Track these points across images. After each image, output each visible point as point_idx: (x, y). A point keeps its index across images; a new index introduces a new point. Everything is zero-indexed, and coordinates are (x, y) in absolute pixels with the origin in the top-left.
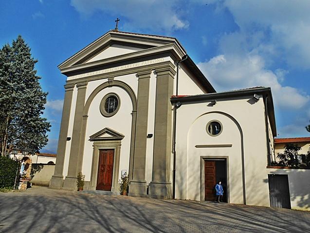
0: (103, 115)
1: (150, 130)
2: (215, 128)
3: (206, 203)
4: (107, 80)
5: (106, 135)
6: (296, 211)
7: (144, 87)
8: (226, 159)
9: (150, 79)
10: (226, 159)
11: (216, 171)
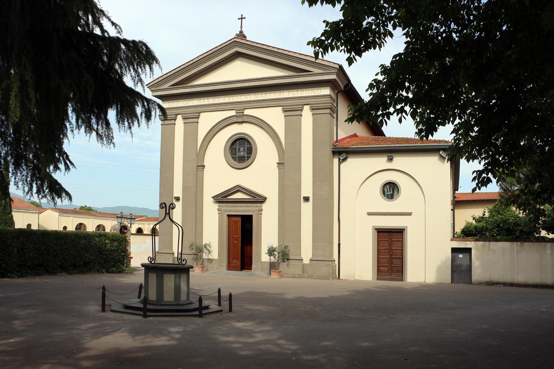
0: (233, 167)
1: (307, 189)
2: (391, 190)
4: (233, 113)
5: (239, 196)
7: (294, 130)
9: (302, 118)
10: (404, 229)
11: (390, 245)
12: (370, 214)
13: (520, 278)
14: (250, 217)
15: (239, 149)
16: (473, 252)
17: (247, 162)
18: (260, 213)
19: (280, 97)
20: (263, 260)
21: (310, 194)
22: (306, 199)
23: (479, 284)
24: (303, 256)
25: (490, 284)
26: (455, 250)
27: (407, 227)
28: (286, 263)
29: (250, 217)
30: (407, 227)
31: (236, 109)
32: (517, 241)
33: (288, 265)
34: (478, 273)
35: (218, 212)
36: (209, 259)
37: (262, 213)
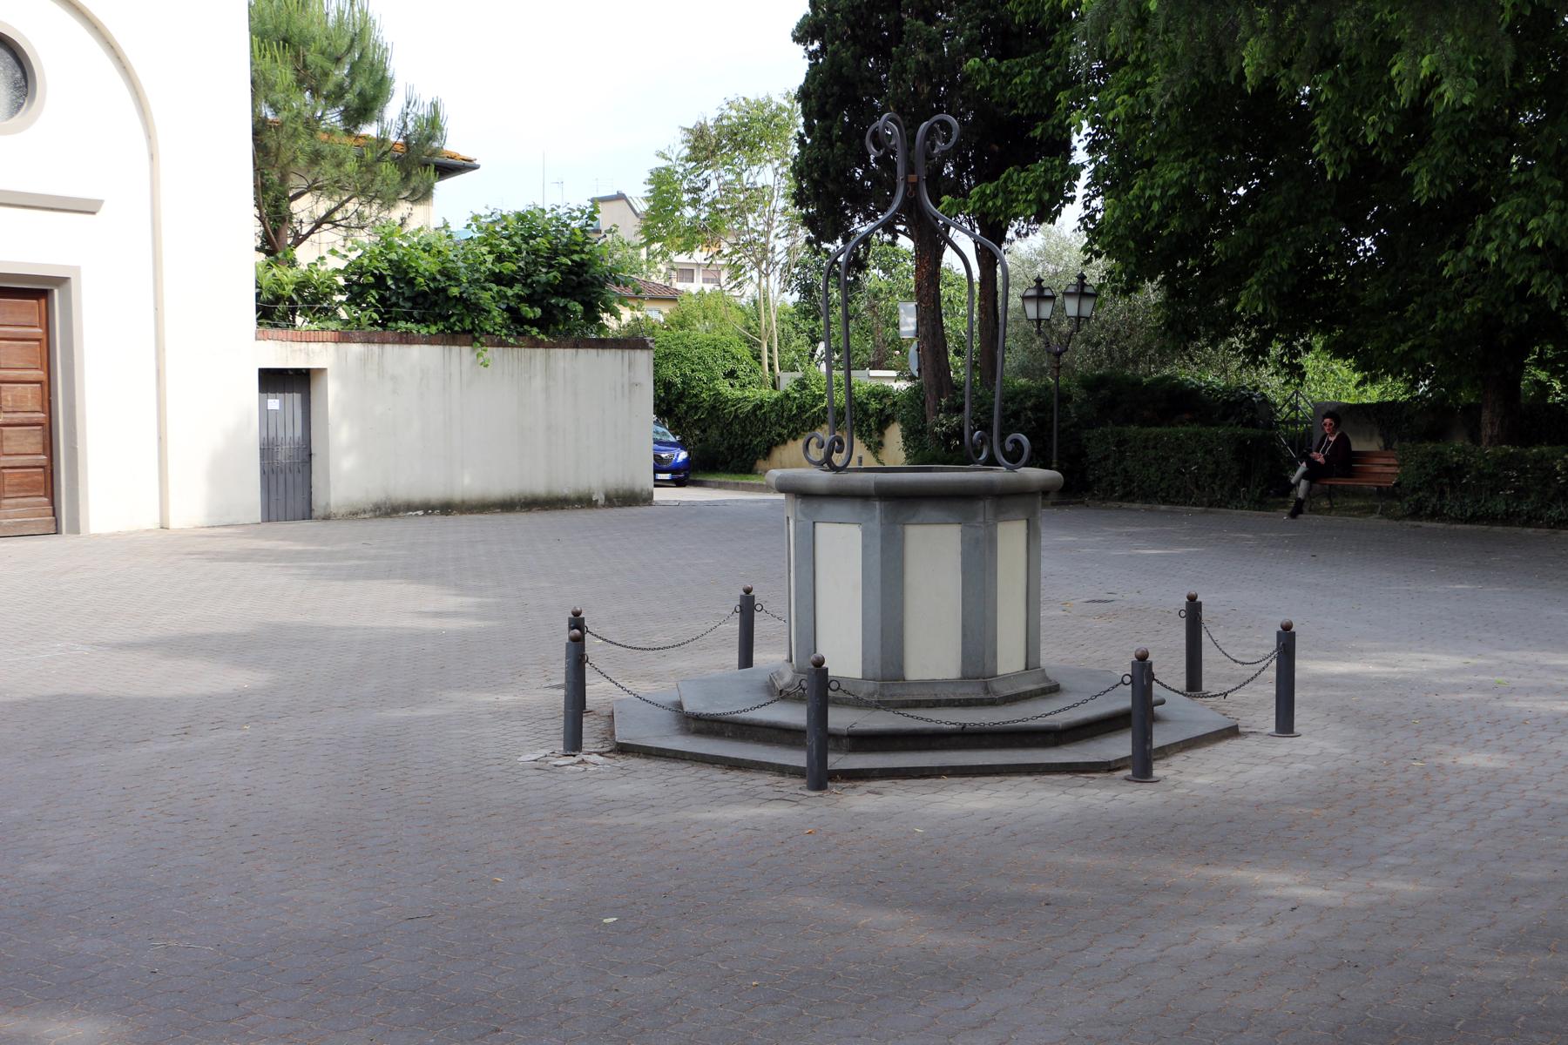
6: (386, 525)
10: (62, 281)
13: (468, 484)
23: (354, 514)
26: (272, 380)
27: (77, 269)
30: (77, 269)
34: (347, 468)
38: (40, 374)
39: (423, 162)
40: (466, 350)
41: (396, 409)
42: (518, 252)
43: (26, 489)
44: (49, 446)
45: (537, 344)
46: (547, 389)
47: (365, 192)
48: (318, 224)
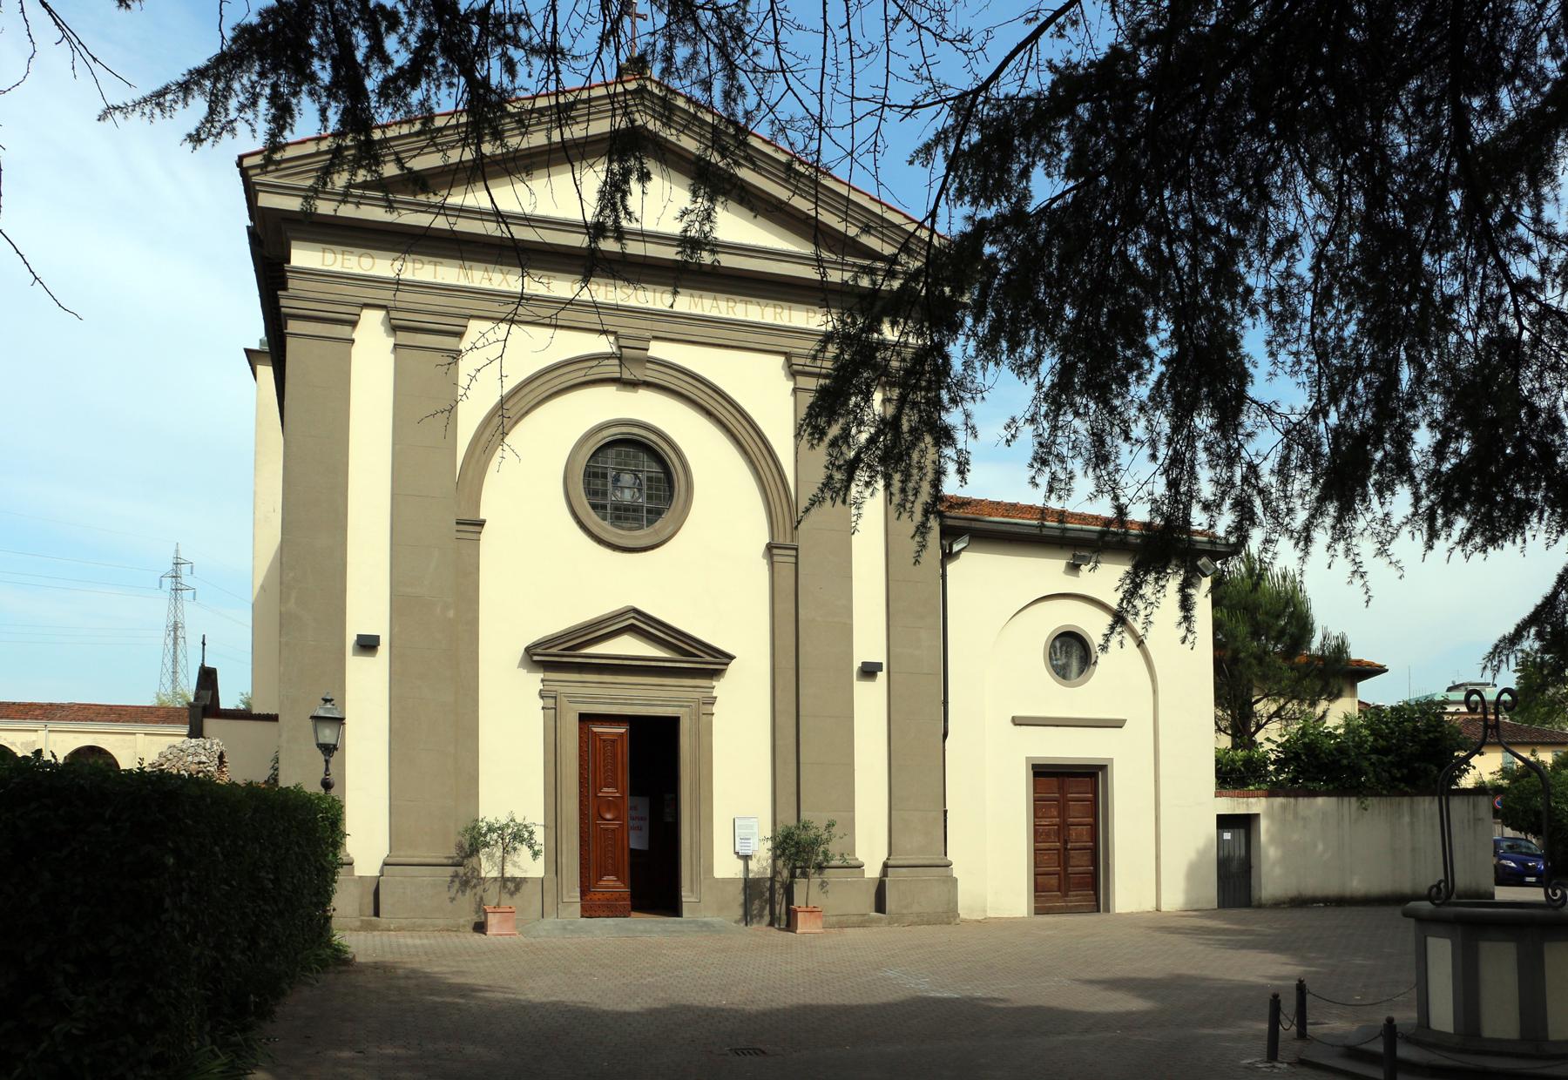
1: (869, 643)
3: (626, 852)
4: (603, 344)
5: (627, 646)
6: (1298, 915)
8: (1034, 766)
12: (1018, 722)
13: (1357, 885)
14: (672, 724)
15: (617, 479)
16: (1264, 824)
17: (646, 531)
18: (705, 709)
19: (778, 322)
20: (719, 872)
21: (379, 625)
22: (367, 645)
23: (1277, 905)
24: (861, 854)
25: (1300, 902)
26: (1224, 822)
28: (815, 880)
29: (672, 724)
31: (621, 331)
32: (1350, 795)
33: (823, 885)
35: (541, 703)
36: (504, 880)
37: (715, 709)
38: (1090, 820)
39: (1341, 671)
40: (1353, 799)
41: (1302, 842)
42: (1393, 732)
43: (1081, 886)
44: (1095, 861)
45: (1404, 794)
46: (1412, 824)
47: (1294, 695)
48: (1270, 718)
